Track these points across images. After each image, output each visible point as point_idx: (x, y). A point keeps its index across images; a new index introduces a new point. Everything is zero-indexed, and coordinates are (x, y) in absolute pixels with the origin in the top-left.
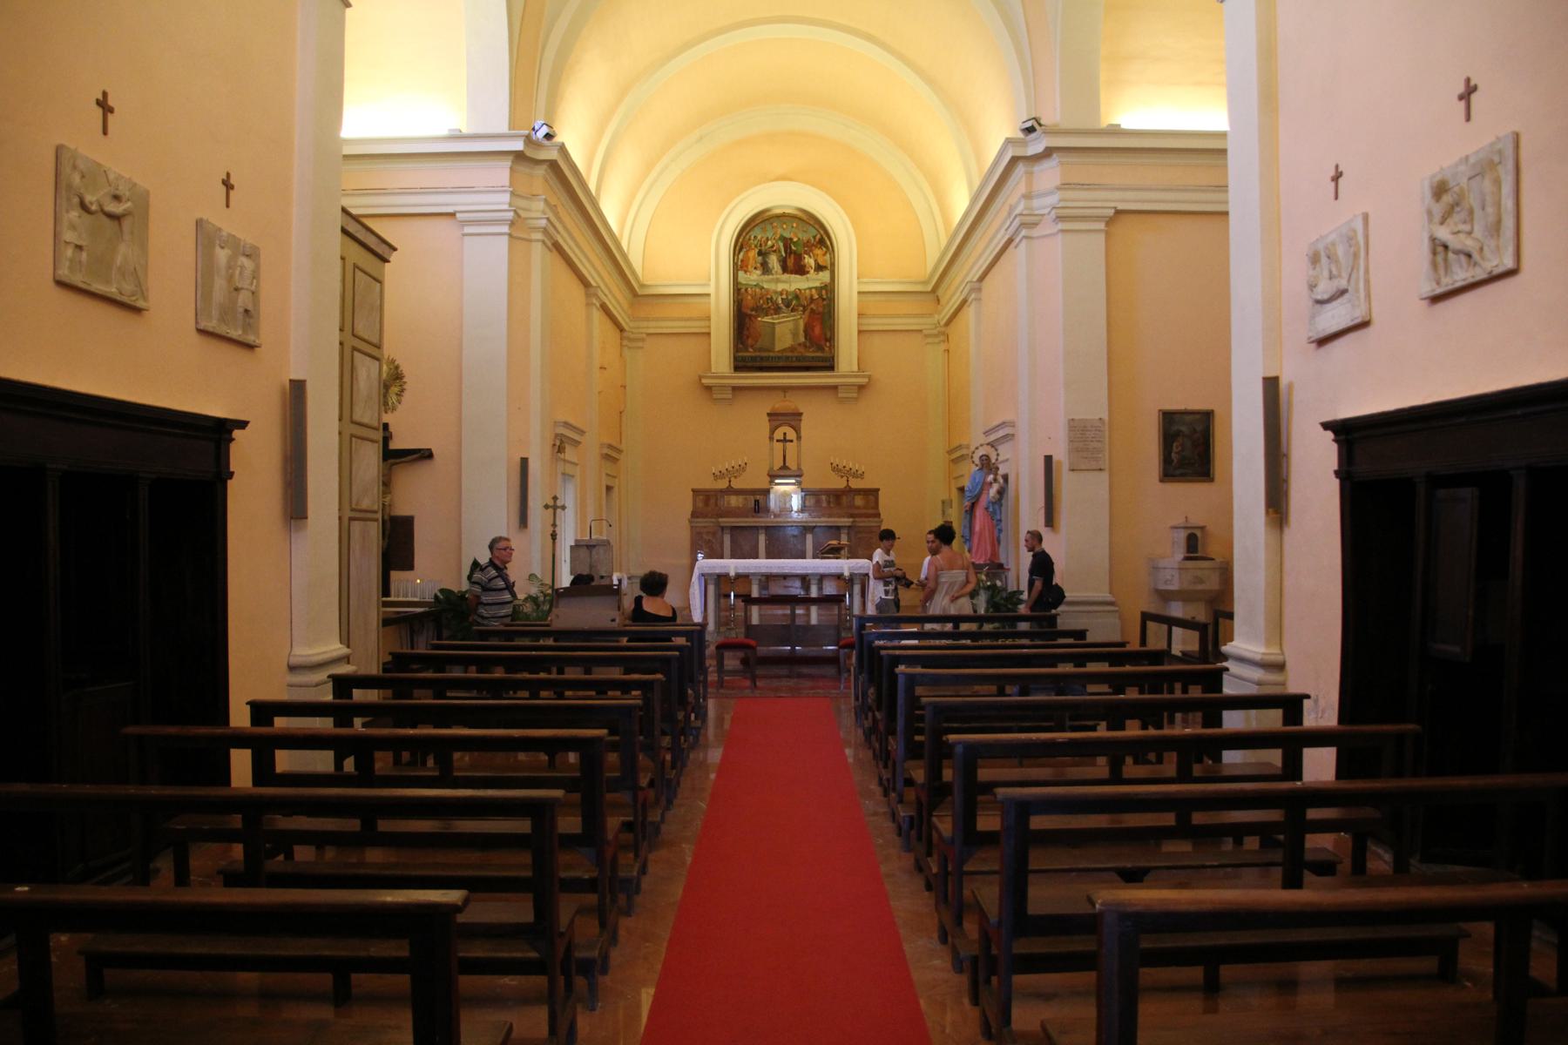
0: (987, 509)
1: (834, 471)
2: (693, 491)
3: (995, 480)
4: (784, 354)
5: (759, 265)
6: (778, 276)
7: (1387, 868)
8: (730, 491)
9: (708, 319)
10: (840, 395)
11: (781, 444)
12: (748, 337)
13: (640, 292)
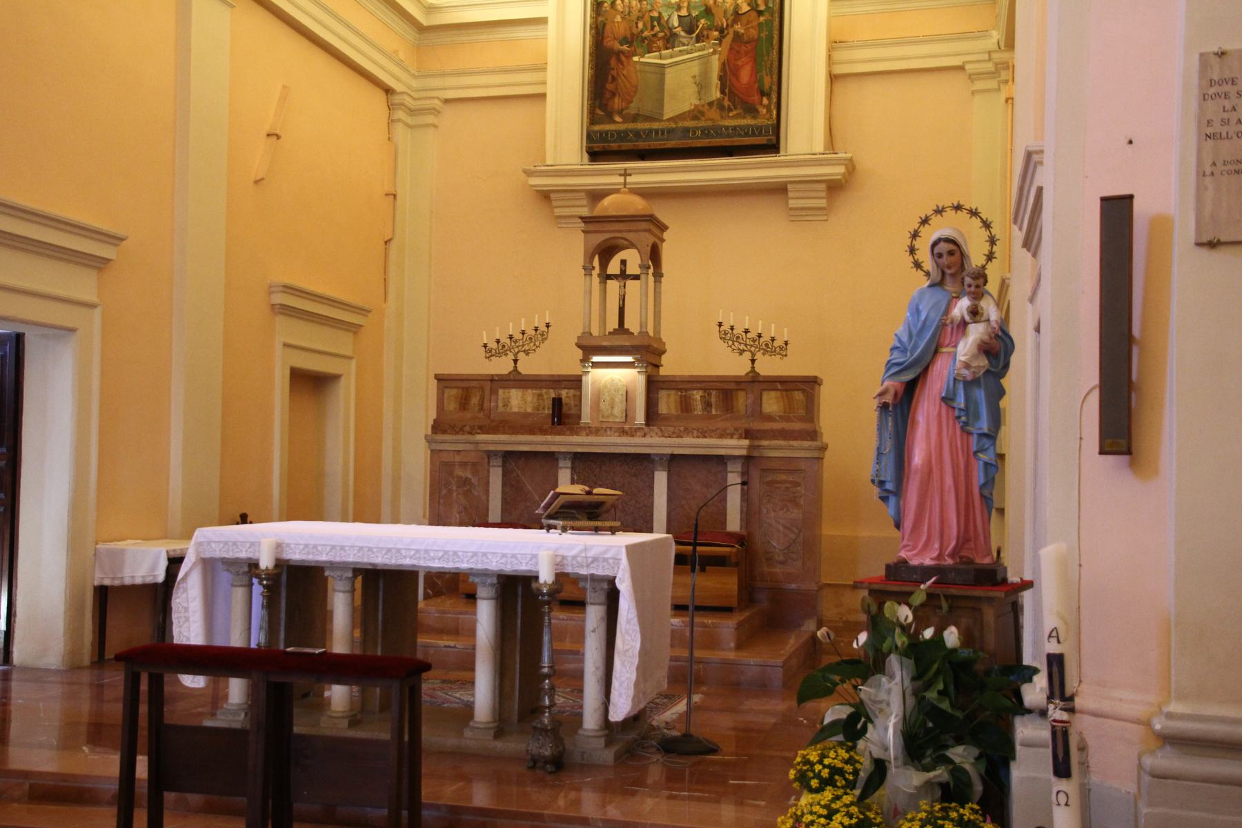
0: (947, 400)
2: (440, 379)
3: (975, 313)
4: (680, 124)
8: (516, 380)
9: (542, 68)
10: (792, 203)
12: (614, 94)
13: (424, 21)
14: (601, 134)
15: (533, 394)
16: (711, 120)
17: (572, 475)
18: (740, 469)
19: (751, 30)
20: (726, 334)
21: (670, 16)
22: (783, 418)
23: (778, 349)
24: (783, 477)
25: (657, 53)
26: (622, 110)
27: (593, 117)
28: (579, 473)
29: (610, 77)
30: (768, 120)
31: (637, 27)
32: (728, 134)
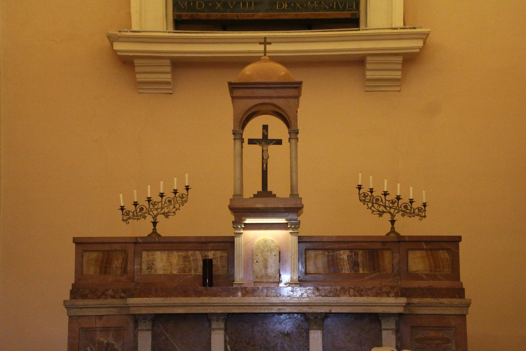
1: (364, 201)
2: (79, 242)
10: (369, 75)
11: (258, 148)
15: (179, 256)
17: (225, 336)
18: (394, 327)
20: (365, 196)
22: (431, 277)
23: (417, 211)
24: (432, 334)
28: (231, 333)
32: (314, 8)
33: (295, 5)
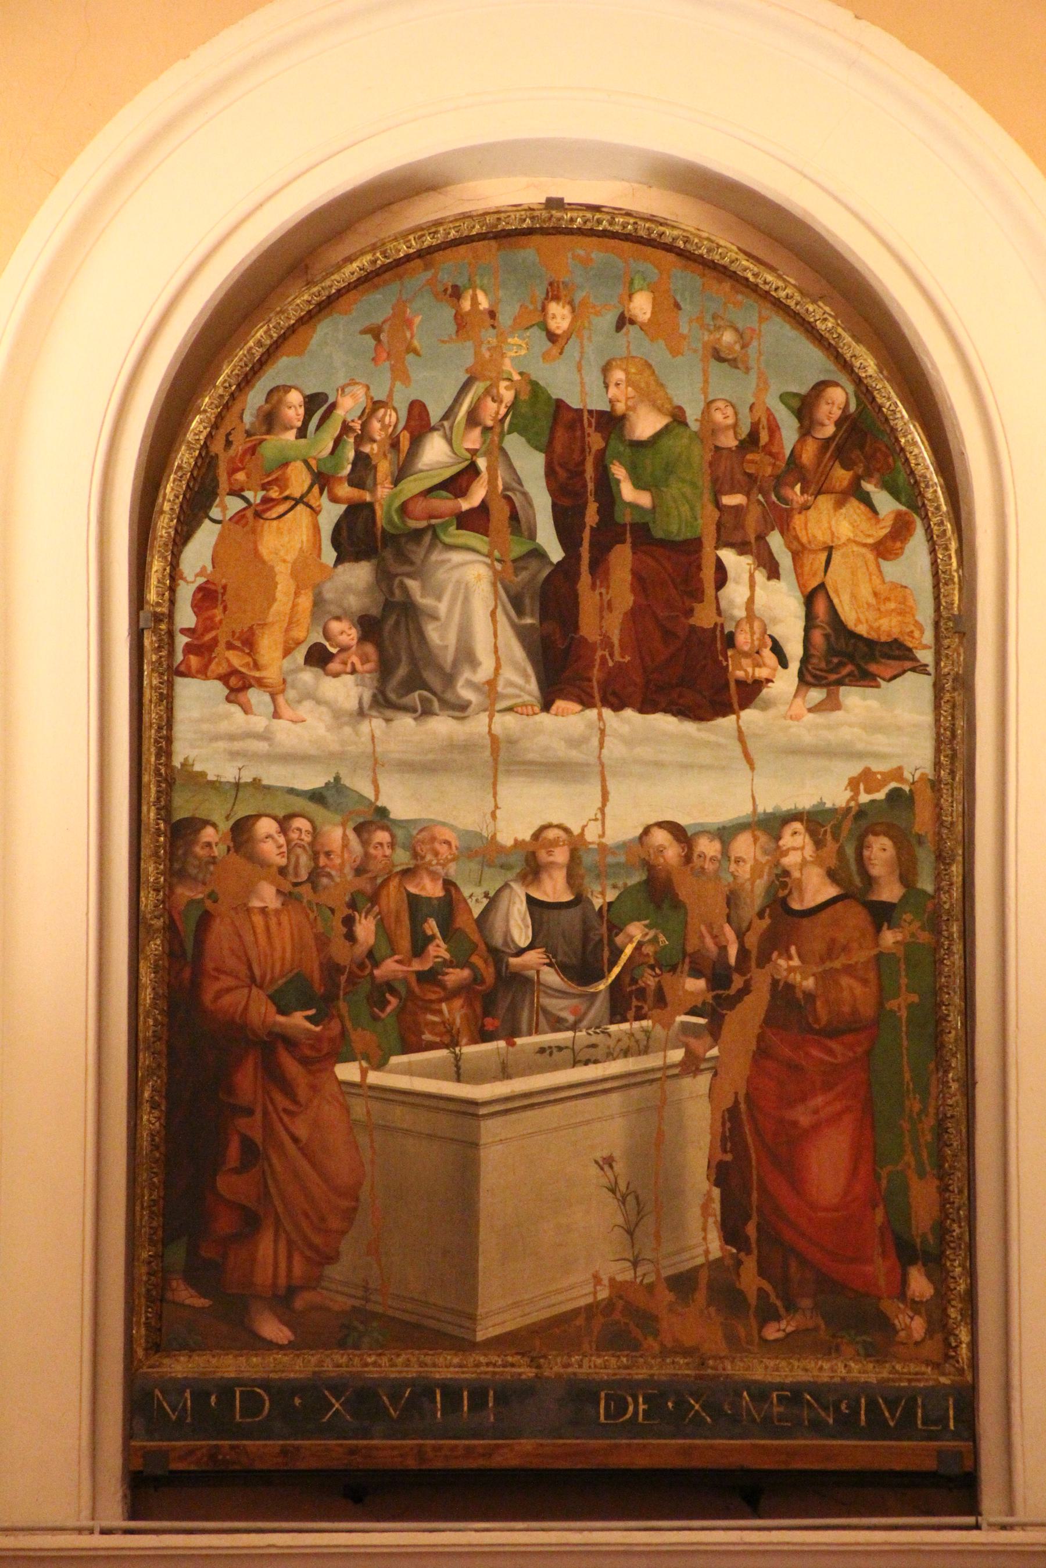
4: (555, 1367)
5: (346, 633)
6: (506, 723)
7: (533, 699)
14: (201, 1395)
16: (687, 1352)
19: (845, 981)
21: (493, 902)
25: (443, 1053)
26: (292, 1291)
27: (160, 1316)
29: (234, 1149)
30: (936, 1366)
31: (351, 937)
32: (767, 1419)
33: (681, 1404)
